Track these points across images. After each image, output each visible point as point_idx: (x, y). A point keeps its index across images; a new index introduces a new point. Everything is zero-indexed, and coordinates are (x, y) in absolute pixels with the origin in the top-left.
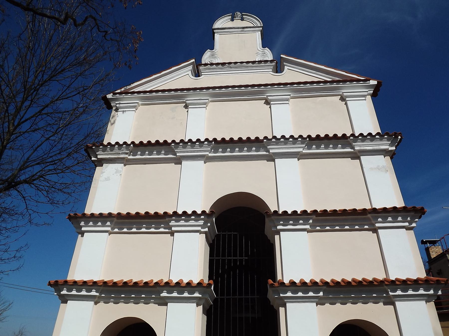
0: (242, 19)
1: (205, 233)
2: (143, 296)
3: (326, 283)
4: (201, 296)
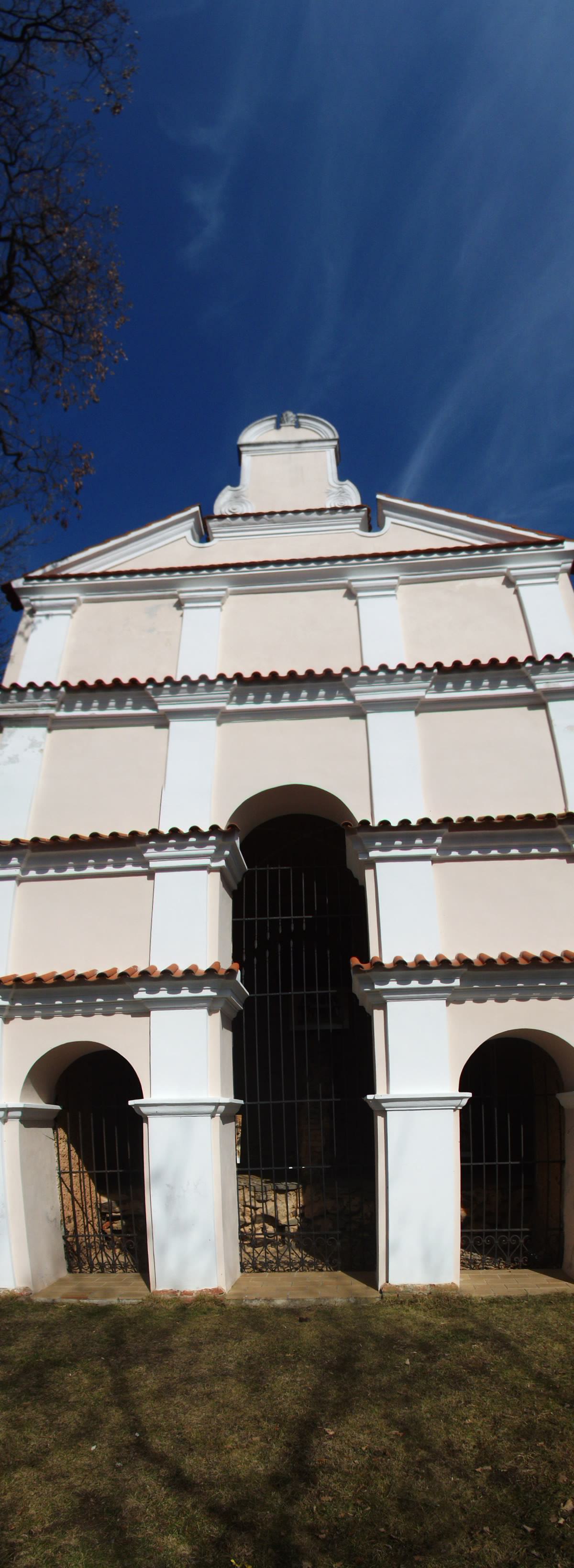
0: (298, 425)
1: (220, 870)
2: (99, 1000)
3: (466, 963)
4: (215, 994)
